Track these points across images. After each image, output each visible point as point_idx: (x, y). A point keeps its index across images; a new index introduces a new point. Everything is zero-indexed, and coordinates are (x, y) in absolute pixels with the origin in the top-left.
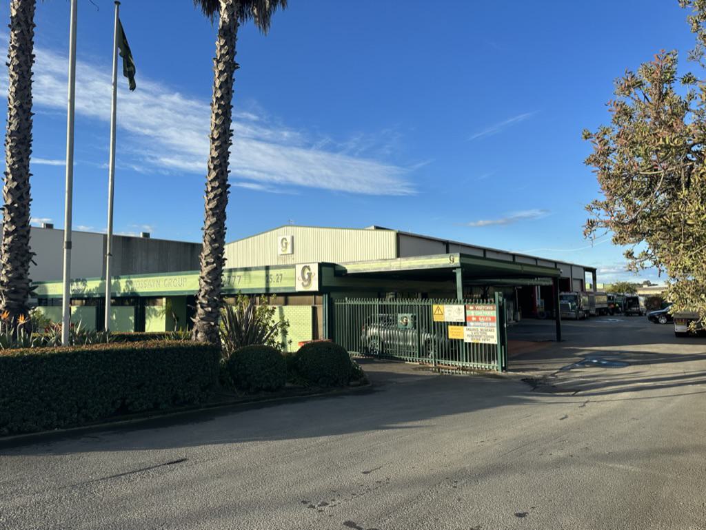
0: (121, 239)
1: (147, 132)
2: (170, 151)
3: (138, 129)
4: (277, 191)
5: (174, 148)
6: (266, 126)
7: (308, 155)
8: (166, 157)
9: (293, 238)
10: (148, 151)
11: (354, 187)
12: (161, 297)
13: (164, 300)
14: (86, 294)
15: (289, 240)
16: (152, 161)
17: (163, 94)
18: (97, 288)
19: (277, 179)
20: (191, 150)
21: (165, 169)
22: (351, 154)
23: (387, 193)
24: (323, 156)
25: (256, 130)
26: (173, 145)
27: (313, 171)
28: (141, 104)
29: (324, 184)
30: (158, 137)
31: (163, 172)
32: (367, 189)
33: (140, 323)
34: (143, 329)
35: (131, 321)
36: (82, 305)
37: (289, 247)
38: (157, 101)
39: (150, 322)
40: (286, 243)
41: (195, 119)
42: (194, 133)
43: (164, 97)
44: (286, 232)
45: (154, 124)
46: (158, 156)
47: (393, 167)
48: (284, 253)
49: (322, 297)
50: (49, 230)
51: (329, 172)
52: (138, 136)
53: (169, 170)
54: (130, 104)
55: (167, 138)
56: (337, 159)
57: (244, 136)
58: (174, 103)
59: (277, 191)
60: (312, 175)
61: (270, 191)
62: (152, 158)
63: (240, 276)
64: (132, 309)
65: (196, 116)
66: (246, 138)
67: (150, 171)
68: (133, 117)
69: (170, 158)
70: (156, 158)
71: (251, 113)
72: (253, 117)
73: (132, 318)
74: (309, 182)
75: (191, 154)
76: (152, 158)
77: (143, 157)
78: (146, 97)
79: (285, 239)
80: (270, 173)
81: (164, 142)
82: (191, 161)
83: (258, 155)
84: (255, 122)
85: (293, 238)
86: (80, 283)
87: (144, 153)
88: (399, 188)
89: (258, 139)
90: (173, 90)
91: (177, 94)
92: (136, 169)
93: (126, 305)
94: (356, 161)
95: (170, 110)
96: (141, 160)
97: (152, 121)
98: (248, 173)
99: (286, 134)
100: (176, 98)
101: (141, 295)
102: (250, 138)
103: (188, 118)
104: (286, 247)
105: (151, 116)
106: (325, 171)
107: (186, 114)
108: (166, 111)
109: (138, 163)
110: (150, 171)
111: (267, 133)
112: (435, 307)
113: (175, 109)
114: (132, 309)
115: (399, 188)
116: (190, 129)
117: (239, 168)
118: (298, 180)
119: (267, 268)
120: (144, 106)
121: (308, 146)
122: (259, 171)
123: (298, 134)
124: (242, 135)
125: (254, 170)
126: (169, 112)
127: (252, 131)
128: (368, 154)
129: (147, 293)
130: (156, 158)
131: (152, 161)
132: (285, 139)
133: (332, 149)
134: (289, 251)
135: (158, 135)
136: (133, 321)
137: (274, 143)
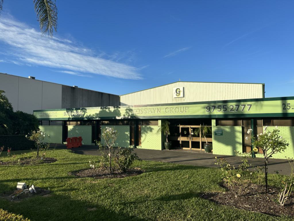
0: (70, 88)
1: (20, 46)
2: (31, 55)
3: (15, 44)
4: (82, 76)
5: (33, 54)
6: (76, 46)
7: (96, 60)
8: (29, 58)
9: (184, 88)
10: (20, 55)
11: (116, 75)
12: (157, 120)
13: (160, 122)
14: (86, 118)
15: (181, 89)
16: (22, 59)
17: (26, 28)
18: (97, 114)
19: (82, 70)
20: (41, 55)
21: (29, 64)
22: (115, 60)
23: (131, 78)
24: (102, 61)
25: (71, 47)
26: (32, 53)
27: (98, 67)
28: (16, 33)
29: (104, 73)
30: (25, 48)
31: (28, 65)
32: (122, 76)
33: (136, 139)
34: (137, 142)
35: (127, 135)
36: (77, 125)
37: (182, 93)
38: (24, 32)
39: (146, 135)
40: (179, 92)
41: (43, 41)
42: (42, 48)
43: (27, 30)
44: (180, 85)
45: (23, 42)
46: (25, 57)
47: (132, 67)
48: (178, 97)
49: (261, 121)
50: (33, 80)
51: (106, 68)
52: (15, 47)
53: (31, 64)
54: (11, 32)
55: (29, 49)
56: (108, 62)
57: (66, 50)
58: (32, 33)
59: (82, 76)
60: (98, 69)
61: (78, 75)
62: (23, 58)
63: (251, 105)
64: (128, 127)
65: (42, 40)
66: (66, 51)
67: (22, 64)
68: (12, 38)
69: (32, 58)
70: (24, 58)
71: (68, 39)
72: (70, 42)
73: (128, 133)
74: (97, 72)
75: (41, 57)
76: (23, 58)
77: (18, 57)
78: (18, 29)
79: (179, 89)
80: (78, 67)
81: (28, 51)
82: (41, 60)
83: (73, 59)
84: (70, 44)
85: (184, 88)
86: (79, 111)
87: (18, 55)
88: (135, 76)
89: (72, 52)
90: (31, 27)
91: (33, 29)
92: (15, 63)
93: (121, 125)
94: (117, 64)
95: (30, 36)
96: (17, 59)
97: (22, 41)
98: (68, 67)
99: (85, 50)
100: (33, 31)
101: (141, 118)
102: (69, 51)
103: (39, 40)
104: (179, 94)
105: (21, 38)
106: (103, 67)
107: (38, 39)
108: (28, 36)
109: (16, 60)
110: (22, 64)
111: (77, 49)
112: (129, 126)
113: (32, 36)
114: (128, 127)
115: (135, 76)
116: (40, 45)
117: (64, 64)
118: (92, 71)
119: (284, 99)
120: (18, 33)
121: (95, 56)
122: (73, 66)
123: (90, 50)
124: (65, 49)
125: (71, 65)
126: (30, 37)
127: (69, 48)
128: (122, 61)
129: (184, 116)
130: (24, 58)
131: (22, 59)
132: (85, 52)
133: (106, 58)
134: (181, 95)
135: (25, 47)
136: (129, 135)
137: (80, 54)
